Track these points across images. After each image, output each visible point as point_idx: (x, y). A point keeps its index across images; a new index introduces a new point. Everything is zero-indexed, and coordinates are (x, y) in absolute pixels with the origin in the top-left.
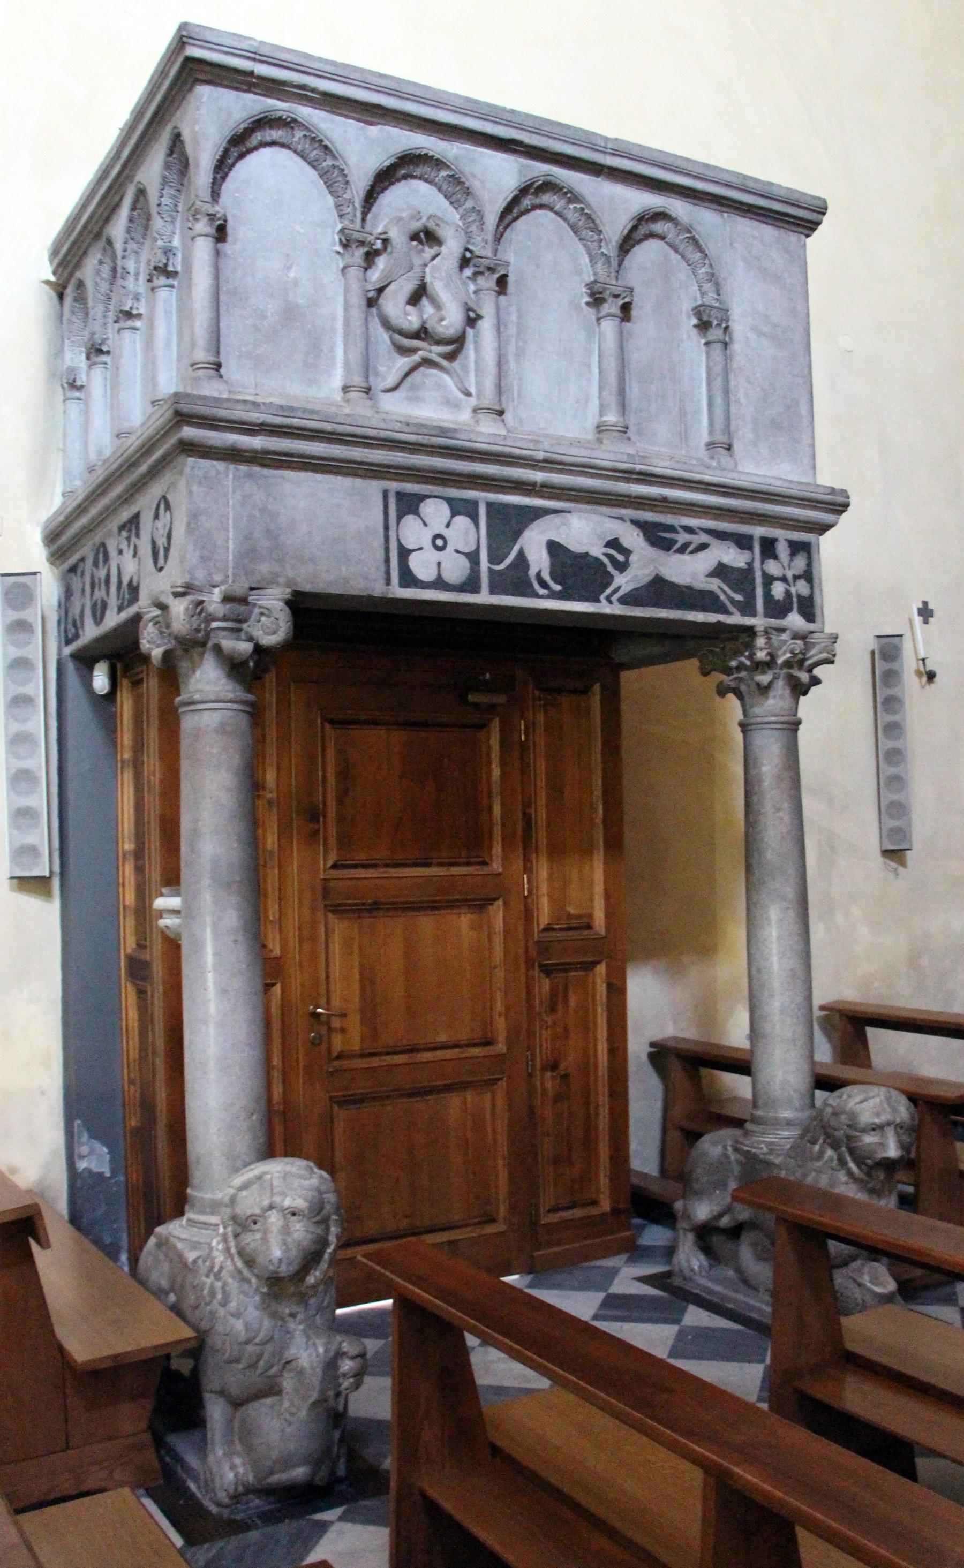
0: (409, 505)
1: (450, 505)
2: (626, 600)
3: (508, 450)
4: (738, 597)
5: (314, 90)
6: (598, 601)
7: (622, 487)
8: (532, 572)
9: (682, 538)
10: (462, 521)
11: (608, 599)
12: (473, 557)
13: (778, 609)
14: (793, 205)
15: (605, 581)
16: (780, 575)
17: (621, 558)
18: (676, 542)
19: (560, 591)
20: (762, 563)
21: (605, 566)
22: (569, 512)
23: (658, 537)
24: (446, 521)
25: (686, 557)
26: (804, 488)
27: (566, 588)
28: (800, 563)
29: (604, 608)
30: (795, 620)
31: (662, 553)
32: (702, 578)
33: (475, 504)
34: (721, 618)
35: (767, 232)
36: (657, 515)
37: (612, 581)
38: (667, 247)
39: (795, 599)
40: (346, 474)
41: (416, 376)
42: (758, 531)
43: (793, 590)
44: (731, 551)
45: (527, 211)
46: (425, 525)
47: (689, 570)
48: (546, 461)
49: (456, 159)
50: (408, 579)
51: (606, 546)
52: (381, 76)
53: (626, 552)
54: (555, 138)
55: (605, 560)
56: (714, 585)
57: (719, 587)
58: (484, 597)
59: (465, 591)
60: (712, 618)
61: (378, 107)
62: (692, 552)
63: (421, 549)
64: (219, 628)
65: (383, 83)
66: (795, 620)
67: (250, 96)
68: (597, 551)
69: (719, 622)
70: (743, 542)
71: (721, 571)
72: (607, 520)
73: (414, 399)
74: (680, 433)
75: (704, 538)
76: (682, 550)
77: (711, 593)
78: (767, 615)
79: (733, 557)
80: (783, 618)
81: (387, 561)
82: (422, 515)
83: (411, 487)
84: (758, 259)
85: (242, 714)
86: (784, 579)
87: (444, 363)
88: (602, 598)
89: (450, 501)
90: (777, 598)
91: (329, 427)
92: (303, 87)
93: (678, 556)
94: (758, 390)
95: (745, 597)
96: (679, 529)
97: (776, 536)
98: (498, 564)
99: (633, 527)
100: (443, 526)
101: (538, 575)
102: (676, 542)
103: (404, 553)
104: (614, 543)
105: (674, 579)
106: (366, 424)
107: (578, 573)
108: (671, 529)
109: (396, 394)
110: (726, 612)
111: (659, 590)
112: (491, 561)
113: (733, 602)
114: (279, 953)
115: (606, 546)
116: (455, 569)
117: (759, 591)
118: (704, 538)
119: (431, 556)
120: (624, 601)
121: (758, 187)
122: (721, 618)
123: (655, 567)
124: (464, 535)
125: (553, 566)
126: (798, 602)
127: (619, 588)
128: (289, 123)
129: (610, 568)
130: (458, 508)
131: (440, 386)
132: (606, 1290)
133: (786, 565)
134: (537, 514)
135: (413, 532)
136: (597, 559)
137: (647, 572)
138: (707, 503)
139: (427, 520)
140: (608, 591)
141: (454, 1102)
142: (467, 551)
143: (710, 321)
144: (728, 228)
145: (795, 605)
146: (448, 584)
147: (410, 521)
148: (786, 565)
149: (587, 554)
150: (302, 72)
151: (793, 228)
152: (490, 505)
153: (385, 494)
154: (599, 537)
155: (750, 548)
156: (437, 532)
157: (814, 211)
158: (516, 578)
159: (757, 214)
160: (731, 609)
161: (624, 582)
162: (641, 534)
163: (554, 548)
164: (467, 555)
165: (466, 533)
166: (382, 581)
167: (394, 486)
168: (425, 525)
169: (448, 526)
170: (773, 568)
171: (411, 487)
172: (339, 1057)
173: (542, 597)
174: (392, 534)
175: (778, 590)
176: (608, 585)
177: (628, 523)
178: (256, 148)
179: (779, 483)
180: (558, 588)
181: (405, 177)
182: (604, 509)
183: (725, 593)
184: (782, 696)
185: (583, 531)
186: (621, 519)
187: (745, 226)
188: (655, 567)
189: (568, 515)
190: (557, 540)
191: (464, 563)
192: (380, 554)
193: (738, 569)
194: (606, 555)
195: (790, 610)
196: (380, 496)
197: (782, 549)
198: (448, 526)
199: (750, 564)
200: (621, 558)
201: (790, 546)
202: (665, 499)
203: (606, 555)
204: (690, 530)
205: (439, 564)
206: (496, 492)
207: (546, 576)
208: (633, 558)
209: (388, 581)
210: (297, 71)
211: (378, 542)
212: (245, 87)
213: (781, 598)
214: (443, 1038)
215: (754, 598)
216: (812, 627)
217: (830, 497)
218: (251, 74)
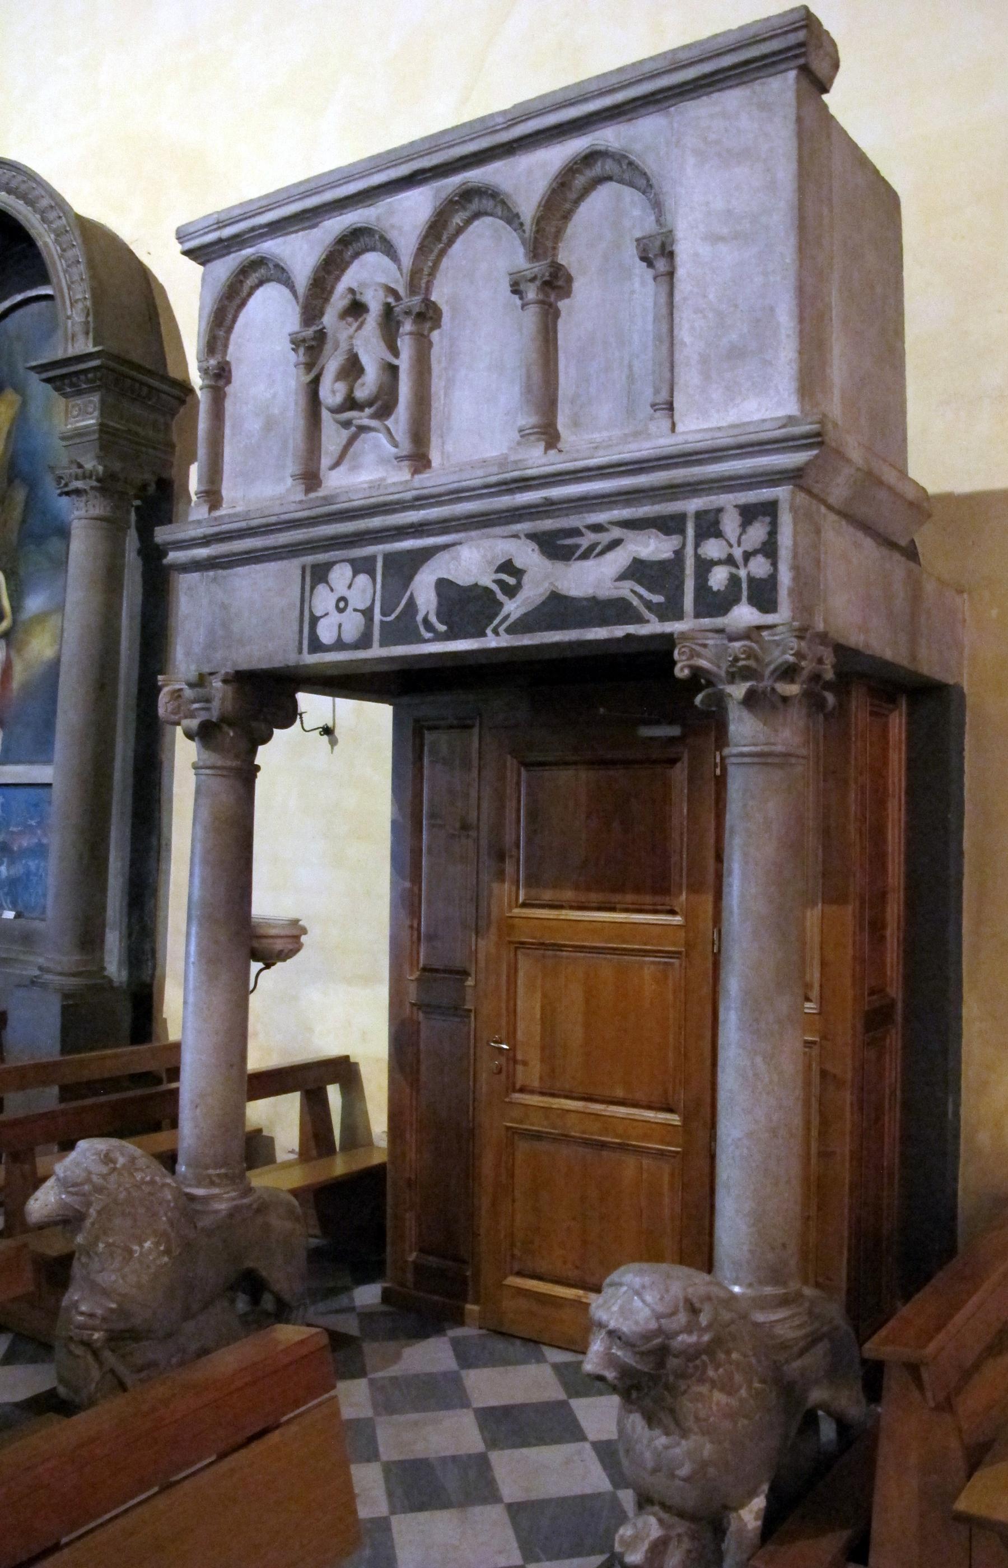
0: (320, 574)
1: (353, 566)
2: (519, 627)
3: (382, 499)
4: (657, 599)
5: (261, 227)
6: (483, 634)
7: (506, 501)
8: (419, 618)
9: (591, 537)
10: (363, 579)
11: (496, 632)
12: (367, 613)
13: (714, 604)
14: (749, 45)
16: (723, 556)
17: (512, 581)
19: (446, 632)
20: (697, 546)
22: (460, 544)
23: (556, 547)
24: (348, 582)
25: (589, 564)
26: (736, 432)
27: (450, 628)
28: (757, 533)
29: (491, 641)
30: (744, 614)
31: (560, 565)
32: (609, 584)
33: (373, 559)
34: (631, 629)
35: (732, 99)
36: (558, 520)
37: (500, 610)
38: (619, 185)
39: (744, 586)
40: (275, 560)
41: (357, 444)
42: (693, 505)
43: (742, 573)
44: (652, 541)
45: (460, 231)
46: (332, 590)
47: (592, 578)
48: (417, 499)
49: (378, 219)
50: (316, 646)
51: (497, 571)
52: (301, 183)
54: (453, 146)
55: (495, 587)
56: (626, 590)
57: (632, 591)
58: (376, 651)
60: (619, 631)
61: (304, 212)
64: (196, 709)
65: (302, 189)
66: (744, 614)
67: (232, 256)
68: (487, 580)
69: (628, 637)
70: (669, 525)
71: (638, 570)
73: (355, 468)
75: (616, 533)
76: (585, 556)
77: (623, 600)
79: (654, 547)
83: (322, 557)
84: (718, 142)
85: (219, 779)
86: (730, 561)
87: (374, 423)
88: (489, 631)
89: (352, 562)
90: (715, 589)
91: (243, 524)
92: (253, 229)
94: (710, 315)
96: (584, 530)
97: (722, 505)
98: (390, 615)
100: (346, 588)
101: (426, 621)
103: (314, 620)
104: (507, 567)
105: (574, 593)
106: (267, 513)
107: (466, 607)
108: (575, 532)
109: (337, 469)
110: (640, 620)
111: (558, 609)
112: (384, 613)
113: (649, 605)
114: (809, 914)
115: (497, 571)
116: (352, 625)
118: (616, 533)
119: (335, 618)
120: (511, 630)
121: (695, 53)
122: (631, 629)
123: (551, 583)
124: (363, 591)
126: (749, 587)
128: (259, 263)
130: (363, 566)
131: (377, 446)
132: (563, 1405)
133: (733, 541)
134: (426, 554)
135: (323, 600)
136: (487, 590)
137: (541, 590)
138: (600, 492)
140: (496, 622)
141: (631, 1162)
143: (659, 253)
144: (675, 125)
145: (745, 593)
147: (321, 589)
148: (733, 541)
149: (476, 585)
150: (250, 217)
151: (772, 70)
152: (388, 558)
153: (303, 569)
155: (682, 532)
156: (340, 595)
157: (786, 33)
159: (709, 85)
160: (647, 614)
161: (513, 608)
162: (536, 547)
163: (443, 586)
164: (363, 612)
167: (310, 559)
168: (332, 590)
170: (713, 549)
171: (322, 557)
172: (522, 1090)
176: (496, 615)
178: (250, 294)
179: (699, 436)
180: (442, 628)
181: (357, 255)
182: (498, 530)
183: (640, 597)
184: (740, 719)
185: (470, 562)
186: (516, 536)
187: (700, 112)
188: (551, 583)
191: (359, 618)
192: (296, 627)
193: (661, 563)
194: (495, 581)
195: (737, 601)
196: (299, 572)
197: (730, 524)
198: (350, 587)
199: (679, 554)
200: (512, 581)
201: (741, 515)
202: (549, 502)
203: (495, 581)
204: (597, 528)
205: (340, 626)
206: (392, 542)
207: (433, 619)
208: (526, 579)
209: (300, 651)
210: (246, 218)
212: (225, 252)
213: (723, 588)
214: (620, 1093)
216: (770, 619)
217: (783, 431)
218: (220, 240)
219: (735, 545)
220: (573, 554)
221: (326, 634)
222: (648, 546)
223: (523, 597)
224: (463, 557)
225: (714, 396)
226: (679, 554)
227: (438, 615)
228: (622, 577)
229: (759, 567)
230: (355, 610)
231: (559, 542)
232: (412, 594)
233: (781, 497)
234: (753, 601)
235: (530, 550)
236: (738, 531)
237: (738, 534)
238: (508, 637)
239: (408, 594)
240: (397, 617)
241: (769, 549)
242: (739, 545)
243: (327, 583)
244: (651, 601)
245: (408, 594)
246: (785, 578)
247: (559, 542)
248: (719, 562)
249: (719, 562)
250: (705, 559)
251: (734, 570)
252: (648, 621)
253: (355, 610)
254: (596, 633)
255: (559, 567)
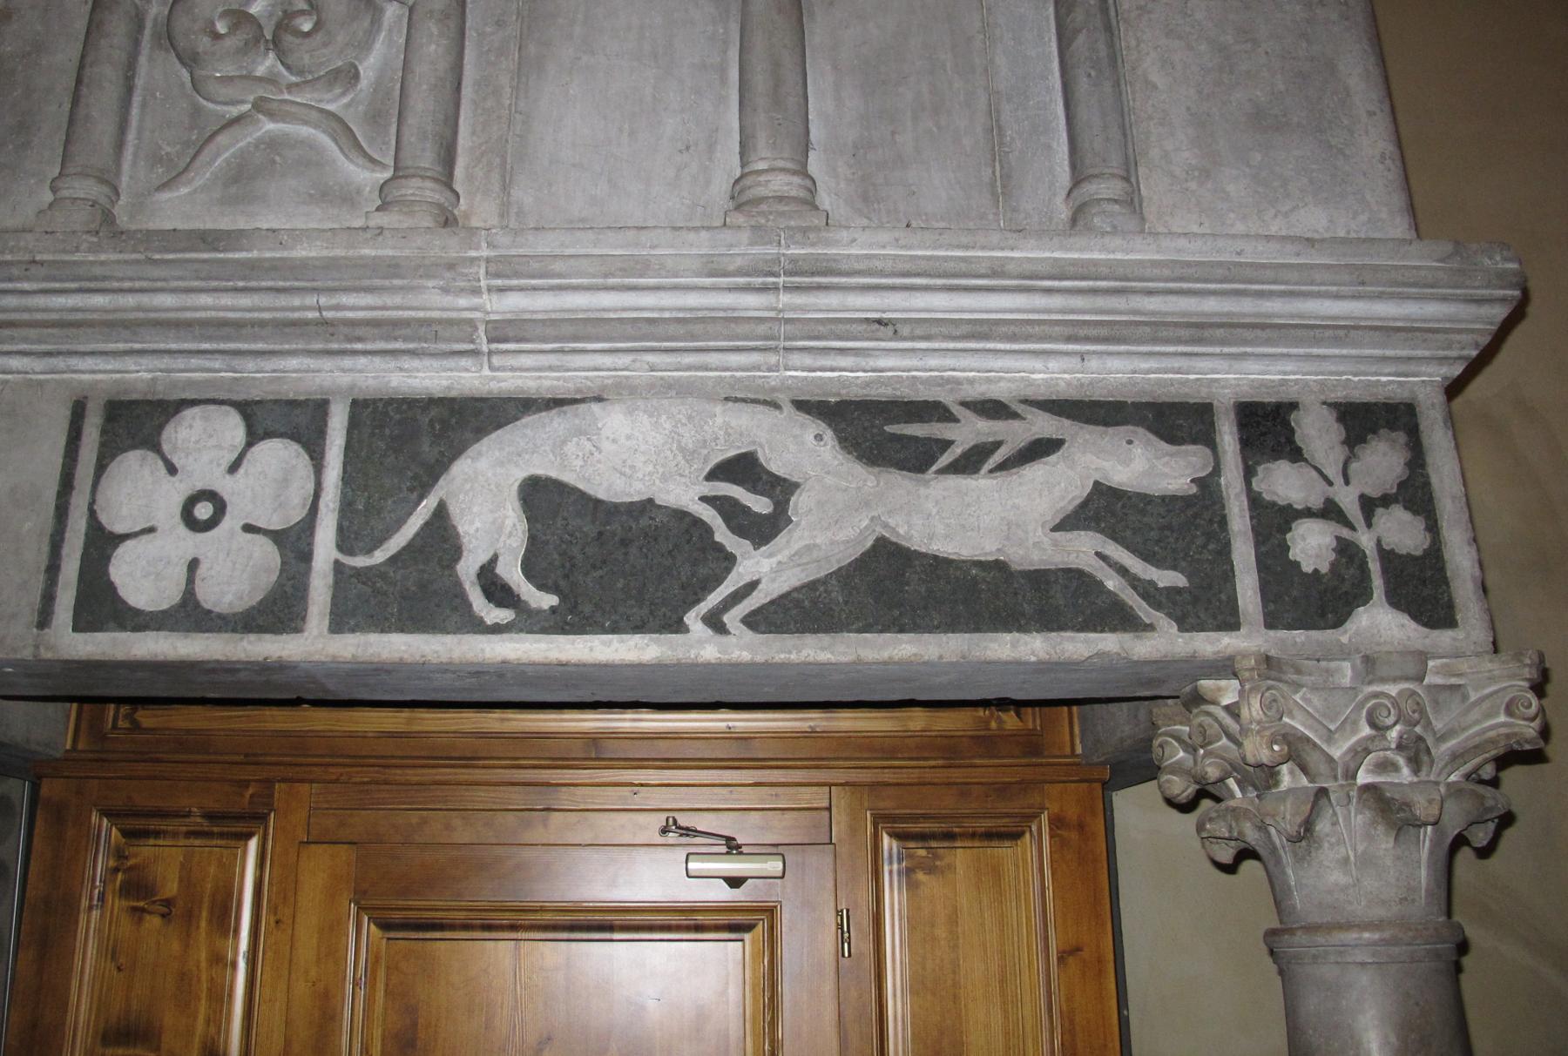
6: (679, 627)
8: (468, 568)
10: (277, 454)
11: (714, 622)
12: (294, 543)
15: (703, 571)
16: (1316, 502)
17: (760, 505)
18: (946, 444)
19: (553, 610)
20: (1249, 473)
21: (708, 530)
25: (980, 484)
28: (1382, 462)
37: (728, 570)
39: (1374, 567)
43: (1365, 540)
46: (172, 470)
50: (101, 605)
51: (712, 476)
53: (781, 489)
55: (708, 514)
56: (1082, 549)
58: (314, 644)
59: (262, 630)
62: (1003, 467)
63: (151, 530)
68: (685, 493)
70: (1177, 421)
71: (1103, 509)
72: (718, 409)
74: (993, 184)
75: (1044, 425)
76: (970, 463)
78: (1271, 622)
79: (1147, 467)
80: (1338, 624)
81: (53, 569)
82: (166, 447)
86: (1330, 511)
88: (693, 618)
93: (954, 481)
95: (1189, 577)
96: (957, 410)
99: (802, 417)
102: (946, 444)
103: (102, 542)
104: (742, 468)
111: (889, 583)
112: (346, 542)
113: (1148, 592)
115: (712, 476)
116: (236, 570)
117: (1243, 554)
118: (1044, 425)
120: (753, 621)
122: (1109, 642)
124: (274, 481)
125: (534, 542)
126: (1385, 571)
127: (752, 586)
129: (723, 535)
133: (1333, 472)
135: (137, 492)
136: (681, 515)
137: (847, 533)
139: (176, 460)
140: (713, 599)
142: (276, 524)
145: (1377, 583)
146: (138, 612)
148: (1333, 472)
154: (689, 455)
158: (424, 586)
161: (767, 569)
162: (829, 435)
163: (540, 496)
164: (277, 537)
165: (285, 482)
166: (29, 615)
168: (172, 470)
169: (234, 468)
170: (1284, 483)
173: (497, 629)
174: (79, 503)
175: (1311, 546)
177: (788, 409)
180: (548, 601)
183: (1123, 571)
189: (595, 407)
190: (553, 474)
191: (266, 554)
192: (37, 554)
193: (1169, 501)
194: (704, 499)
195: (1361, 595)
197: (1318, 433)
198: (234, 468)
199: (1208, 486)
200: (760, 505)
203: (704, 499)
207: (512, 573)
208: (800, 503)
209: (44, 618)
211: (40, 519)
213: (1324, 568)
215: (1229, 576)
219: (1338, 480)
220: (932, 460)
221: (141, 577)
222: (1127, 462)
223: (796, 546)
224: (606, 432)
225: (1231, 188)
226: (1208, 486)
227: (530, 569)
228: (1069, 523)
229: (1400, 531)
230: (249, 528)
231: (888, 429)
232: (441, 512)
233: (1421, 397)
234: (1396, 599)
235: (809, 437)
236: (1340, 453)
237: (1342, 459)
238: (749, 635)
239: (427, 507)
240: (393, 560)
241: (1414, 493)
242: (1347, 482)
243: (157, 448)
244: (1152, 583)
245: (427, 507)
246: (1461, 559)
247: (888, 429)
248: (1308, 513)
249: (1308, 513)
250: (1274, 504)
251: (1345, 533)
252: (1150, 627)
253: (249, 528)
254: (1014, 645)
255: (898, 484)
